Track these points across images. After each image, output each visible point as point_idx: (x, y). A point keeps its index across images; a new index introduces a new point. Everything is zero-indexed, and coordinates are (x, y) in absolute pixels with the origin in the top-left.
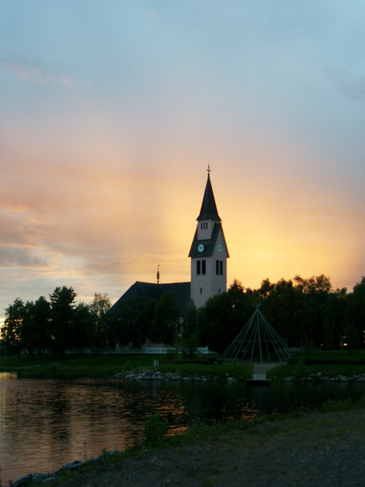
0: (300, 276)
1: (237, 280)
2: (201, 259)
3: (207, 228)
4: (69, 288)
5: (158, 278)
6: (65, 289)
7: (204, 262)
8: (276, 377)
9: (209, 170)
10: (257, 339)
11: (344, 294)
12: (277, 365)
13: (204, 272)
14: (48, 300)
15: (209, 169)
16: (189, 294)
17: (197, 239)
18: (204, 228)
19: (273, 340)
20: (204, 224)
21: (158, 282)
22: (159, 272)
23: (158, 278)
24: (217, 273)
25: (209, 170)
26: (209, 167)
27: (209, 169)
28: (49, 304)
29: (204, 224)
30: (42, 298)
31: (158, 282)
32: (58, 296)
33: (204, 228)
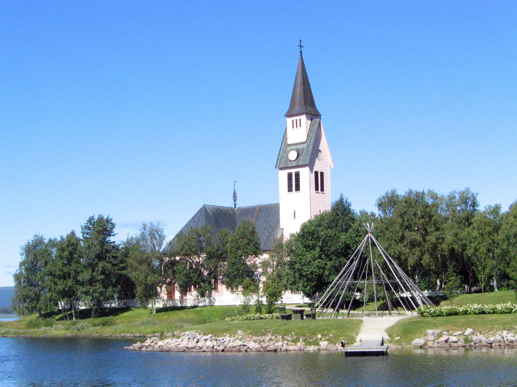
0: (433, 190)
1: (343, 194)
2: (293, 171)
3: (300, 126)
4: (105, 217)
5: (235, 201)
6: (101, 219)
7: (297, 175)
8: (399, 338)
9: (301, 46)
10: (365, 270)
11: (497, 214)
12: (401, 317)
13: (298, 188)
14: (79, 235)
15: (301, 44)
16: (278, 221)
17: (287, 143)
18: (297, 127)
19: (308, 93)
20: (296, 120)
21: (235, 205)
22: (236, 192)
23: (235, 201)
24: (317, 189)
25: (301, 46)
26: (301, 41)
27: (301, 44)
28: (79, 240)
29: (296, 120)
30: (73, 233)
31: (235, 205)
32: (92, 228)
33: (297, 127)
